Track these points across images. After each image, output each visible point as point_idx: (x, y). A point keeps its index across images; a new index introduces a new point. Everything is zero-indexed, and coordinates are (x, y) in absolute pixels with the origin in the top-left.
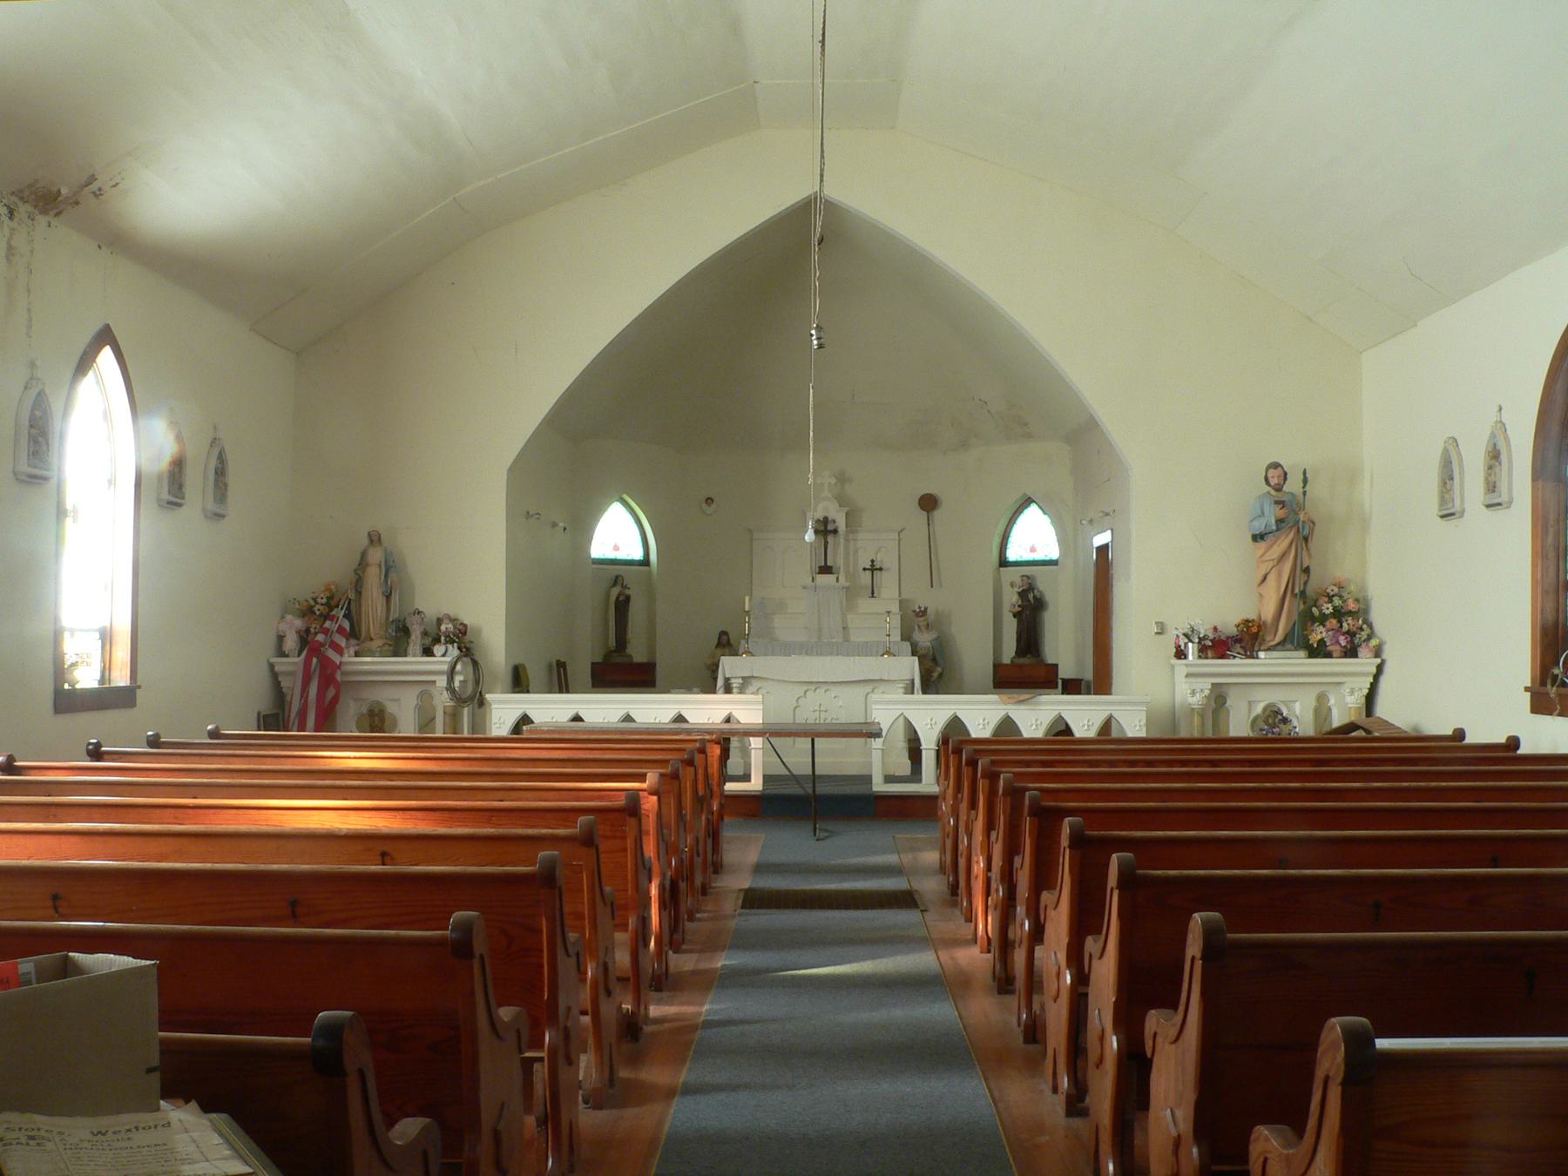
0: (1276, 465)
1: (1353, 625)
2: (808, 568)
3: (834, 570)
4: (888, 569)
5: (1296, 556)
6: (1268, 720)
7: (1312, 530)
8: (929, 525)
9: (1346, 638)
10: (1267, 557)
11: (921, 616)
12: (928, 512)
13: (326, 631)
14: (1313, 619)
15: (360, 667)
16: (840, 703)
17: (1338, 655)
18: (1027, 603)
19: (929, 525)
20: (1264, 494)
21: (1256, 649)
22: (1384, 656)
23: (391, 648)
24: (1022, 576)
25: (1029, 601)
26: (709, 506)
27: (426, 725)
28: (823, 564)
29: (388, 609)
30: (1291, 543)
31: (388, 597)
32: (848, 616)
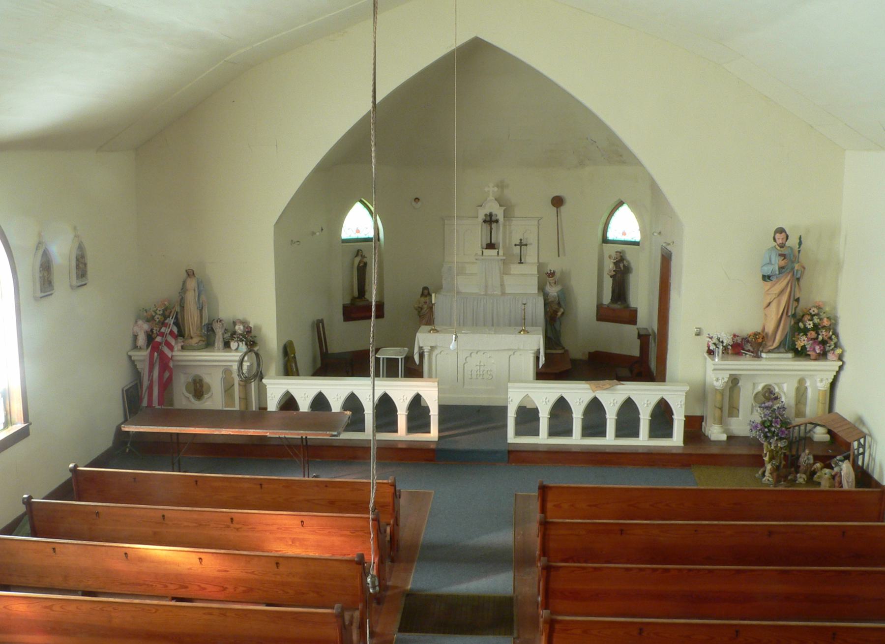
0: (781, 231)
1: (826, 336)
3: (496, 246)
4: (531, 244)
5: (790, 292)
6: (765, 394)
8: (557, 216)
9: (820, 347)
12: (557, 208)
13: (162, 335)
16: (493, 362)
18: (619, 270)
19: (557, 216)
20: (772, 248)
21: (761, 349)
22: (845, 359)
23: (204, 343)
24: (616, 252)
25: (620, 268)
26: (417, 203)
27: (229, 389)
28: (489, 242)
30: (787, 284)
32: (504, 277)
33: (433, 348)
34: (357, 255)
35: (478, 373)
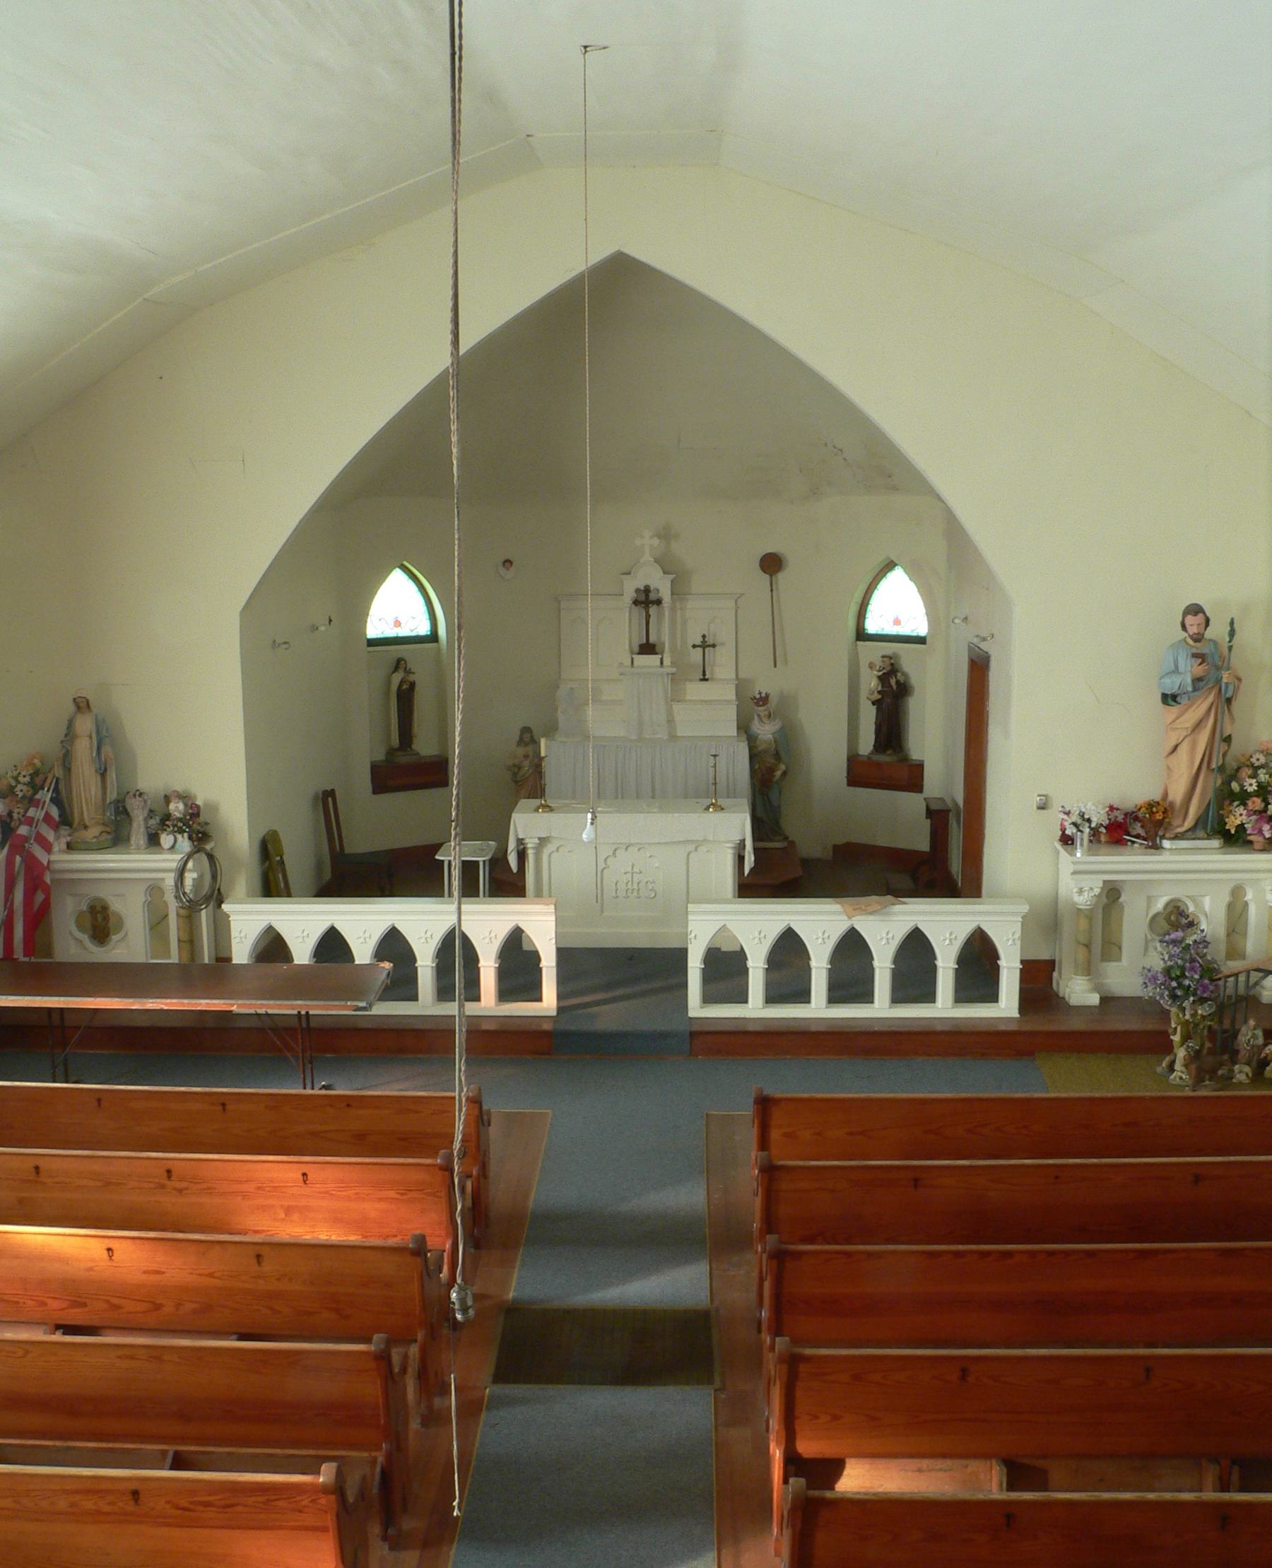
0: (1195, 610)
2: (627, 647)
3: (658, 649)
4: (723, 644)
7: (1236, 690)
8: (772, 590)
10: (1178, 724)
11: (764, 705)
12: (771, 576)
13: (30, 822)
14: (1232, 797)
15: (78, 865)
17: (1259, 848)
24: (883, 657)
25: (891, 687)
26: (508, 570)
28: (645, 641)
29: (104, 793)
30: (1210, 709)
31: (103, 774)
33: (543, 841)
34: (396, 668)
35: (629, 886)
